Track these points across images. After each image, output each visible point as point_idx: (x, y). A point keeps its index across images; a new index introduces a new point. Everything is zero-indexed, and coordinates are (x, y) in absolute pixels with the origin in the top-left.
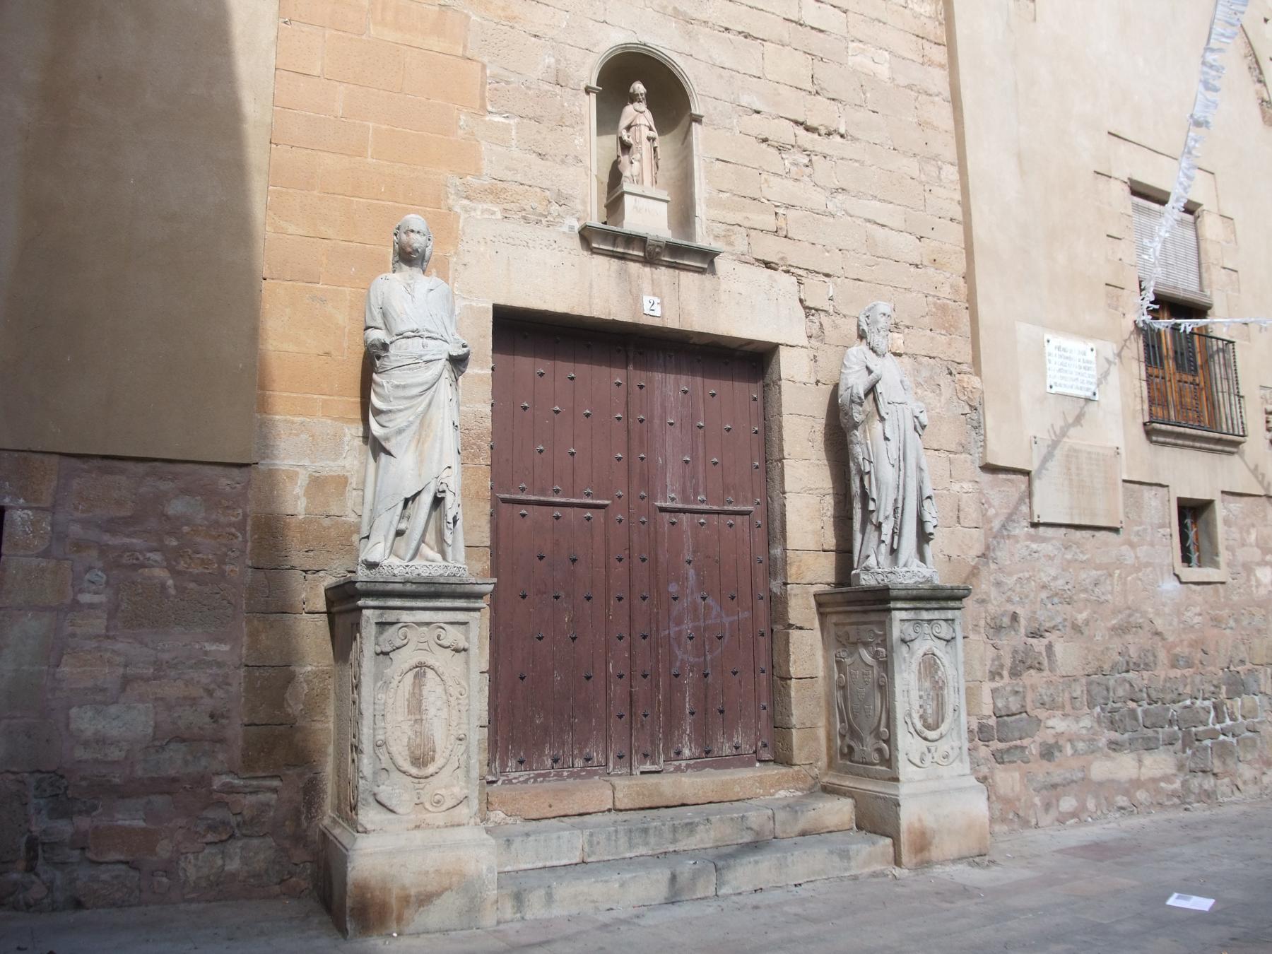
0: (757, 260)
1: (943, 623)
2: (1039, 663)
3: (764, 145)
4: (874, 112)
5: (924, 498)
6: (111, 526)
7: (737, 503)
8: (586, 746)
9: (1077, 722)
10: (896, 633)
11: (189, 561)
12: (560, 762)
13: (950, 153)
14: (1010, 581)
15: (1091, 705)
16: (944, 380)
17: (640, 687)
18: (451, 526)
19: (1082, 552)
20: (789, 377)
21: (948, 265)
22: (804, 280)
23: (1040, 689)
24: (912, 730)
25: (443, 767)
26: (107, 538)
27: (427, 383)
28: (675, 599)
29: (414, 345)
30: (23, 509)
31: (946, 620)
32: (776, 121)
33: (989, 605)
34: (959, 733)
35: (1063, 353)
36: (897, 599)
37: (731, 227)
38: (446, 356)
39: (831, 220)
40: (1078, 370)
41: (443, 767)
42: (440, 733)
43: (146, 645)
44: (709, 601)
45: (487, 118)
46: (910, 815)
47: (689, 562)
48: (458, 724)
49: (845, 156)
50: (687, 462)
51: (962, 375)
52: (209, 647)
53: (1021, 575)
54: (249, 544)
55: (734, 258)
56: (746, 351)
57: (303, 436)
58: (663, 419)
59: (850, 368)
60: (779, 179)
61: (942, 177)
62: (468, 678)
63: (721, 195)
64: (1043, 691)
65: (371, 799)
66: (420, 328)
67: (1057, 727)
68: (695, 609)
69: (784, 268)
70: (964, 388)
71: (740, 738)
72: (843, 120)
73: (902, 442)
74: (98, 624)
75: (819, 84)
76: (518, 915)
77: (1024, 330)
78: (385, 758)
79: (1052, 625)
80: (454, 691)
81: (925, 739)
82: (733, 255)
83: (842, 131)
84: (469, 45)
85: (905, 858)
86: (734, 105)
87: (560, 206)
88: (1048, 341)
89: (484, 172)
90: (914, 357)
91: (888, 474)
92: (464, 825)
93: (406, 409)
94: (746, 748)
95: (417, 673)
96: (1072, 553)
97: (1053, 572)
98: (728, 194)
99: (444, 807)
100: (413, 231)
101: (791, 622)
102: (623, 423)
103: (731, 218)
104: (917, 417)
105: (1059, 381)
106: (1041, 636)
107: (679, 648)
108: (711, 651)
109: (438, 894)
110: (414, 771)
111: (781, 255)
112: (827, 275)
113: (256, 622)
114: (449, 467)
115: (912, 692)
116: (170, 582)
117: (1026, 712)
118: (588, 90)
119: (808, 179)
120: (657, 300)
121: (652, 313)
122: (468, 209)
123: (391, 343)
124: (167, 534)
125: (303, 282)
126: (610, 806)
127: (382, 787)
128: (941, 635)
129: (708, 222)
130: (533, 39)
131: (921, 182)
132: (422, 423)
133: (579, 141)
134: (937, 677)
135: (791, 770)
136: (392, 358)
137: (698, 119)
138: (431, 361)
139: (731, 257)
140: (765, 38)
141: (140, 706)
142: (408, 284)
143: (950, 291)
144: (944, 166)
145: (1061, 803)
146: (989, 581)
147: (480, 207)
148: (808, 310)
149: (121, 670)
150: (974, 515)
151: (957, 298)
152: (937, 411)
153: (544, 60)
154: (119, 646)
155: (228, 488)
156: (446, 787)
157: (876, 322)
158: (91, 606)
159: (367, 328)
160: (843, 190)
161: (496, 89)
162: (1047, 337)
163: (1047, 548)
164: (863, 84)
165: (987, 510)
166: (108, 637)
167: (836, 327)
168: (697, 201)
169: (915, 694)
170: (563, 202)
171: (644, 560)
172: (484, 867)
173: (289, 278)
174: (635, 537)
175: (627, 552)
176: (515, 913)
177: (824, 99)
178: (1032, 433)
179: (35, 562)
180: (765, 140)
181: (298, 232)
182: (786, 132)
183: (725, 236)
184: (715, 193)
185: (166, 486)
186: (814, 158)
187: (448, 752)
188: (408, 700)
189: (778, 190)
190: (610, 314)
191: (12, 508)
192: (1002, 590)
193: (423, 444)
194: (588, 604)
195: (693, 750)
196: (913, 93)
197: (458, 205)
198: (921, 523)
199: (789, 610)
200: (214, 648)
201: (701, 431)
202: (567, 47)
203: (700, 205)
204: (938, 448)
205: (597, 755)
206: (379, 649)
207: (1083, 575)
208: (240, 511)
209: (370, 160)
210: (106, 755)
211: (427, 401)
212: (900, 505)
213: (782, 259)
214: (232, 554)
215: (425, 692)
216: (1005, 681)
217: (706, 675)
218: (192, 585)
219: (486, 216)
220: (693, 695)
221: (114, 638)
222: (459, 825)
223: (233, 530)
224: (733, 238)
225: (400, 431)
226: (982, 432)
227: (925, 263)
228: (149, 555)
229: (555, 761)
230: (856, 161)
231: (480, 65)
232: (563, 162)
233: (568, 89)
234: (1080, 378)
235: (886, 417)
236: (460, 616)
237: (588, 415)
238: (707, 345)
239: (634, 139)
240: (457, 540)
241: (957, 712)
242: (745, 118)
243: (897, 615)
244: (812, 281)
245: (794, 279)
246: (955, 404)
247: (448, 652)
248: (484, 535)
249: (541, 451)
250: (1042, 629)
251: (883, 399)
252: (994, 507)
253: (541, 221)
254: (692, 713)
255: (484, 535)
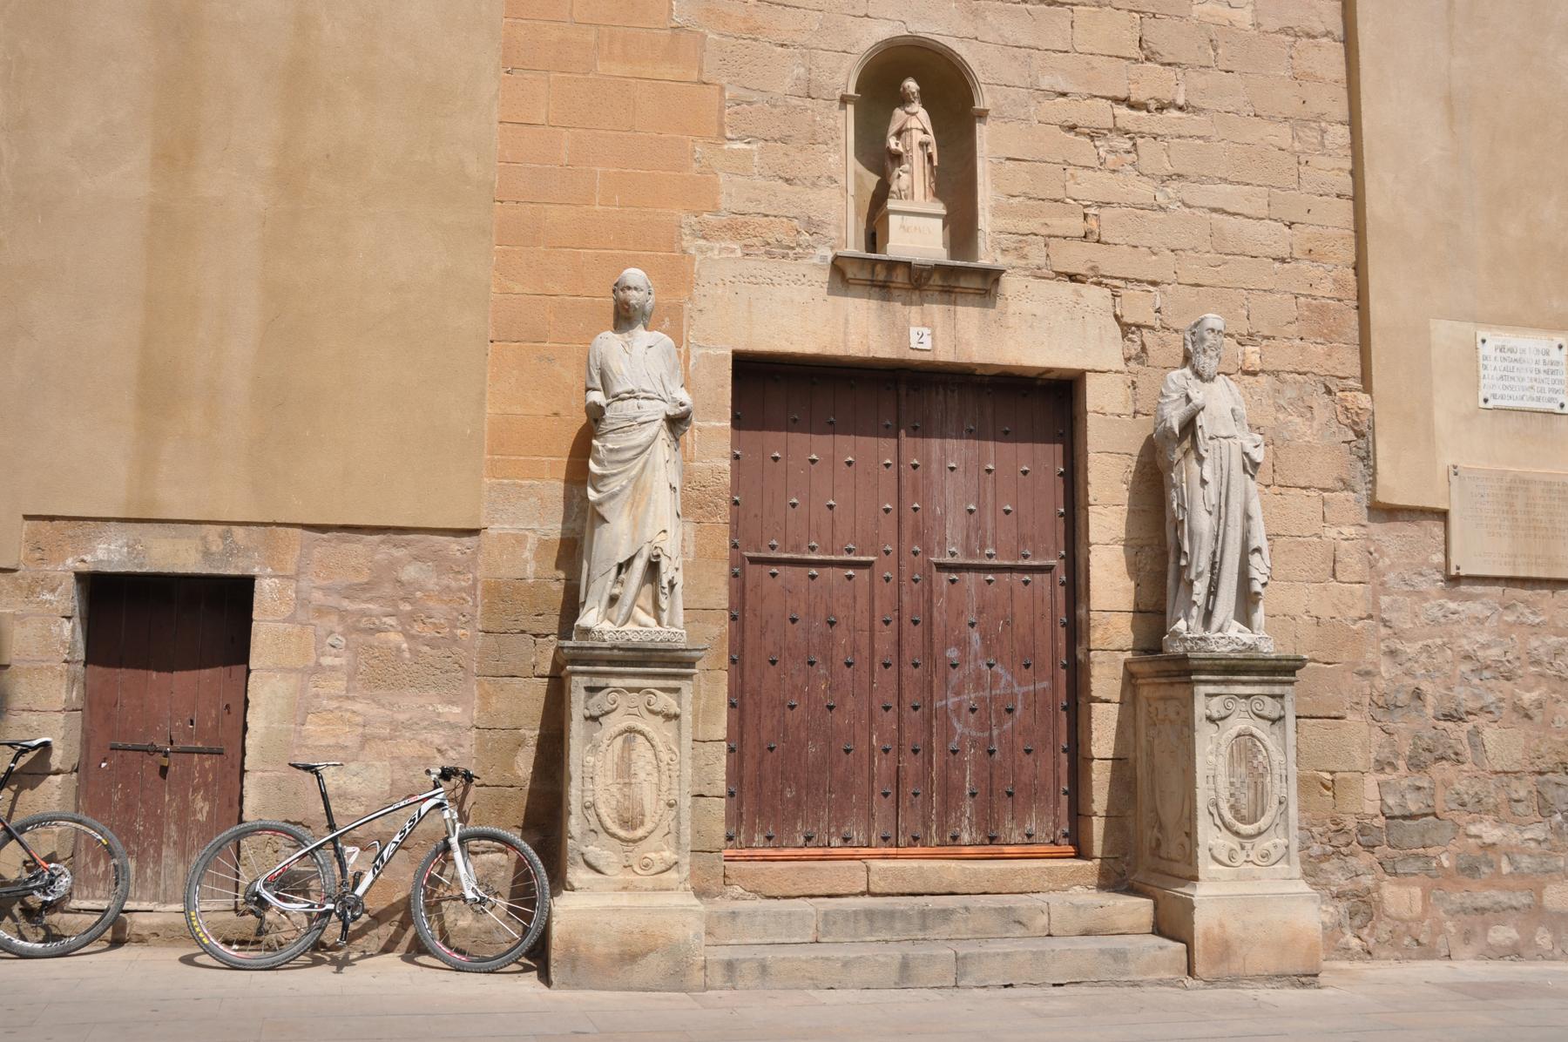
0: (1059, 274)
1: (1268, 700)
2: (1456, 754)
3: (1071, 135)
4: (1227, 72)
5: (1250, 550)
6: (351, 592)
7: (1035, 556)
8: (844, 824)
9: (1521, 832)
10: (1200, 709)
11: (422, 625)
12: (814, 840)
13: (1341, 110)
14: (1410, 649)
15: (1545, 812)
16: (1320, 401)
17: (911, 764)
18: (666, 591)
19: (1534, 613)
20: (1098, 409)
21: (1331, 254)
22: (1122, 292)
23: (1457, 786)
24: (1218, 822)
25: (652, 832)
26: (346, 604)
27: (640, 446)
28: (954, 666)
29: (629, 407)
30: (271, 577)
31: (1273, 696)
32: (1088, 101)
33: (1378, 678)
34: (1286, 829)
35: (1509, 354)
36: (1199, 671)
37: (1024, 238)
38: (663, 416)
39: (1162, 215)
40: (1533, 375)
41: (652, 832)
42: (649, 798)
43: (383, 706)
44: (998, 669)
45: (726, 147)
46: (1204, 920)
47: (972, 625)
48: (669, 789)
49: (1182, 133)
50: (971, 511)
51: (1345, 393)
52: (440, 709)
53: (1429, 642)
54: (480, 608)
55: (1027, 273)
56: (1050, 380)
57: (532, 500)
58: (942, 462)
59: (1167, 397)
60: (1090, 172)
61: (1326, 142)
62: (679, 745)
63: (1011, 200)
64: (1462, 789)
65: (579, 859)
66: (636, 389)
67: (1484, 835)
68: (979, 677)
69: (1095, 279)
70: (1347, 409)
71: (1034, 825)
72: (1182, 88)
73: (1224, 484)
74: (340, 685)
75: (1149, 48)
76: (729, 984)
77: (1443, 332)
78: (593, 819)
79: (1479, 706)
80: (665, 756)
81: (1237, 834)
82: (1026, 269)
83: (1181, 101)
84: (705, 67)
85: (1199, 969)
86: (1031, 91)
87: (811, 235)
88: (1484, 341)
89: (722, 206)
90: (1275, 373)
91: (1204, 523)
92: (673, 889)
93: (620, 473)
94: (1040, 835)
95: (627, 737)
96: (1516, 614)
97: (1483, 638)
98: (1021, 199)
99: (653, 871)
100: (629, 288)
101: (1093, 694)
102: (893, 469)
103: (1024, 226)
104: (1247, 454)
105: (1499, 392)
106: (1461, 719)
107: (959, 720)
108: (1000, 724)
109: (644, 955)
110: (622, 833)
111: (1090, 264)
112: (1154, 283)
113: (486, 686)
114: (665, 531)
115: (1219, 778)
116: (405, 646)
117: (1435, 814)
118: (844, 100)
119: (1130, 168)
120: (926, 331)
121: (920, 346)
122: (704, 249)
123: (608, 405)
124: (402, 599)
125: (530, 342)
126: (863, 888)
127: (590, 848)
128: (1265, 713)
129: (995, 235)
130: (780, 49)
131: (1294, 153)
132: (635, 488)
133: (833, 158)
134: (1255, 762)
135: (1090, 863)
136: (608, 421)
137: (983, 115)
138: (645, 423)
139: (1023, 273)
140: (1075, 2)
141: (377, 764)
142: (627, 342)
143: (1332, 286)
144: (1330, 128)
145: (1491, 933)
146: (1379, 648)
147: (718, 245)
148: (1126, 329)
149: (360, 730)
150: (1358, 568)
151: (1343, 296)
152: (1307, 439)
153: (793, 71)
154: (357, 707)
155: (458, 553)
156: (655, 851)
157: (1203, 340)
158: (333, 668)
159: (588, 389)
160: (1179, 175)
161: (736, 113)
162: (1481, 335)
163: (1475, 608)
164: (1214, 37)
165: (1377, 561)
166: (348, 698)
167: (1164, 345)
168: (980, 212)
169: (1223, 781)
170: (814, 230)
171: (916, 623)
172: (691, 933)
173: (515, 339)
174: (906, 599)
175: (896, 614)
176: (725, 982)
177: (1157, 66)
178: (1450, 461)
179: (281, 626)
180: (1072, 128)
181: (524, 291)
182: (1101, 114)
183: (1016, 249)
184: (1004, 199)
185: (399, 553)
186: (1139, 141)
187: (657, 818)
188: (617, 764)
189: (1087, 186)
190: (869, 351)
191: (261, 576)
192: (1398, 660)
193: (637, 507)
194: (848, 671)
195: (974, 835)
196: (1288, 38)
197: (692, 244)
198: (1245, 579)
199: (1092, 680)
200: (447, 709)
201: (991, 476)
202: (821, 52)
203: (984, 215)
204: (1307, 484)
205: (858, 834)
206: (587, 713)
207: (1534, 643)
208: (470, 576)
209: (597, 207)
210: (347, 809)
211: (641, 464)
212: (1218, 560)
213: (1092, 268)
214: (463, 619)
215: (634, 756)
216: (1400, 776)
217: (991, 752)
218: (426, 649)
219: (724, 255)
220: (975, 774)
221: (353, 698)
222: (668, 890)
223: (464, 595)
224: (1026, 250)
225: (613, 496)
226: (1372, 463)
227: (1295, 255)
228: (385, 619)
229: (808, 839)
230: (1199, 137)
231: (717, 87)
232: (814, 184)
233: (821, 101)
234: (1536, 385)
235: (1205, 454)
236: (672, 683)
237: (849, 463)
238: (996, 376)
239: (904, 146)
240: (674, 606)
241: (1284, 806)
242: (1047, 103)
243: (1201, 690)
244: (1131, 293)
245: (1107, 292)
246: (1335, 429)
247: (660, 719)
248: (721, 597)
249: (794, 505)
250: (1462, 710)
251: (1203, 433)
252: (1388, 556)
253: (788, 254)
254: (973, 795)
255: (721, 597)
